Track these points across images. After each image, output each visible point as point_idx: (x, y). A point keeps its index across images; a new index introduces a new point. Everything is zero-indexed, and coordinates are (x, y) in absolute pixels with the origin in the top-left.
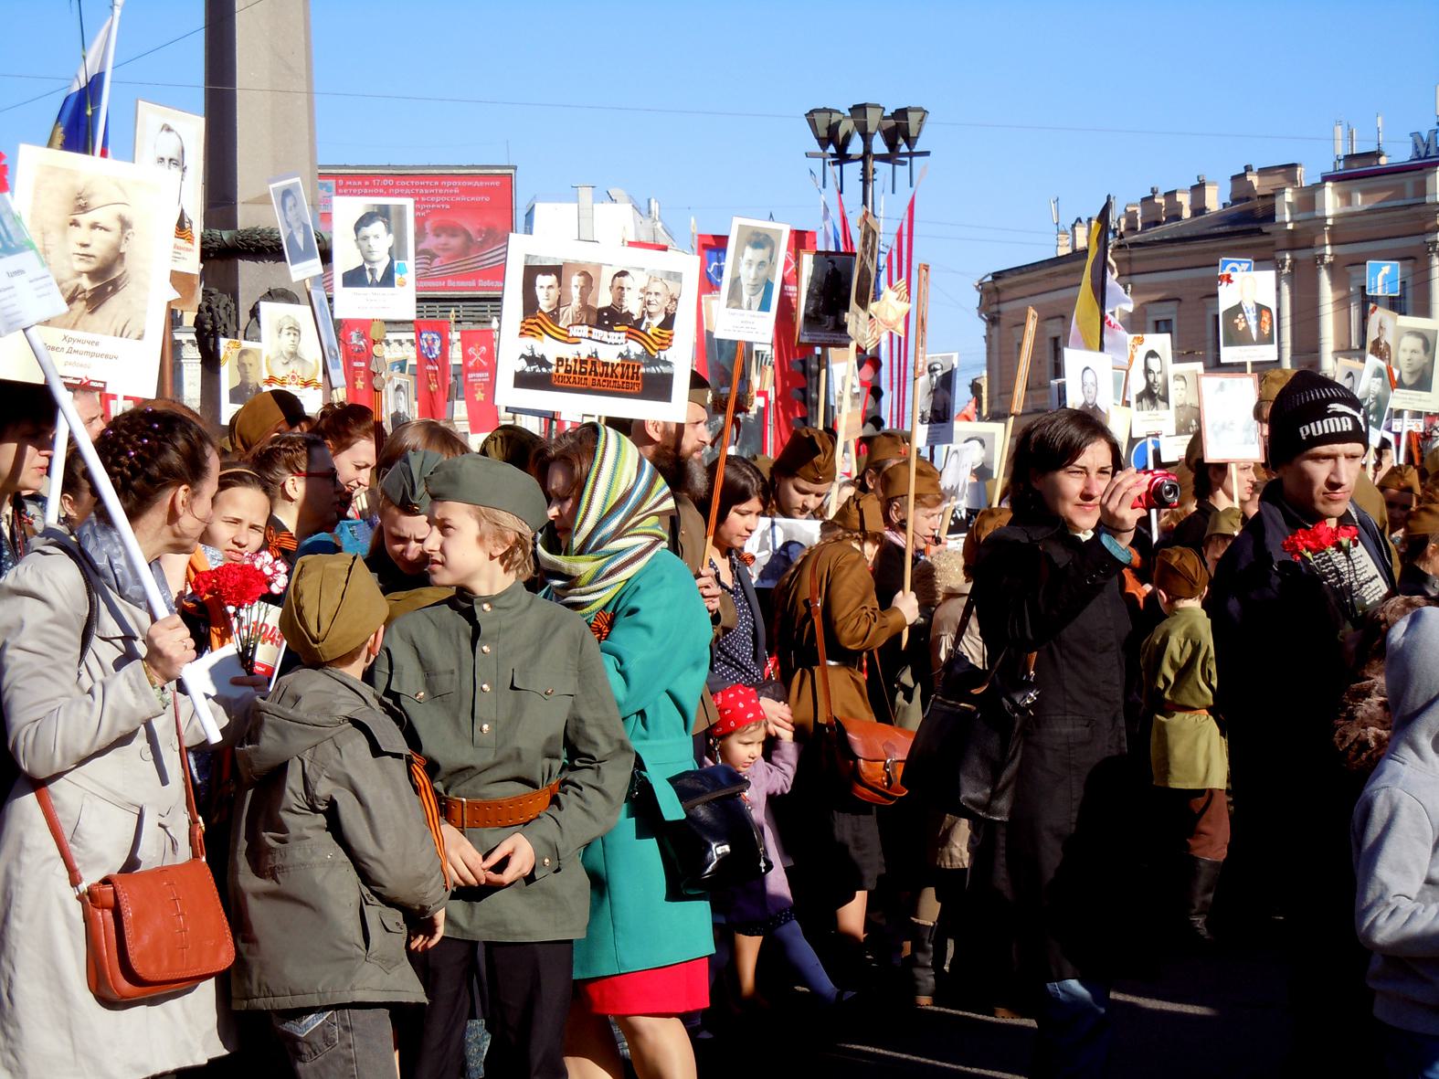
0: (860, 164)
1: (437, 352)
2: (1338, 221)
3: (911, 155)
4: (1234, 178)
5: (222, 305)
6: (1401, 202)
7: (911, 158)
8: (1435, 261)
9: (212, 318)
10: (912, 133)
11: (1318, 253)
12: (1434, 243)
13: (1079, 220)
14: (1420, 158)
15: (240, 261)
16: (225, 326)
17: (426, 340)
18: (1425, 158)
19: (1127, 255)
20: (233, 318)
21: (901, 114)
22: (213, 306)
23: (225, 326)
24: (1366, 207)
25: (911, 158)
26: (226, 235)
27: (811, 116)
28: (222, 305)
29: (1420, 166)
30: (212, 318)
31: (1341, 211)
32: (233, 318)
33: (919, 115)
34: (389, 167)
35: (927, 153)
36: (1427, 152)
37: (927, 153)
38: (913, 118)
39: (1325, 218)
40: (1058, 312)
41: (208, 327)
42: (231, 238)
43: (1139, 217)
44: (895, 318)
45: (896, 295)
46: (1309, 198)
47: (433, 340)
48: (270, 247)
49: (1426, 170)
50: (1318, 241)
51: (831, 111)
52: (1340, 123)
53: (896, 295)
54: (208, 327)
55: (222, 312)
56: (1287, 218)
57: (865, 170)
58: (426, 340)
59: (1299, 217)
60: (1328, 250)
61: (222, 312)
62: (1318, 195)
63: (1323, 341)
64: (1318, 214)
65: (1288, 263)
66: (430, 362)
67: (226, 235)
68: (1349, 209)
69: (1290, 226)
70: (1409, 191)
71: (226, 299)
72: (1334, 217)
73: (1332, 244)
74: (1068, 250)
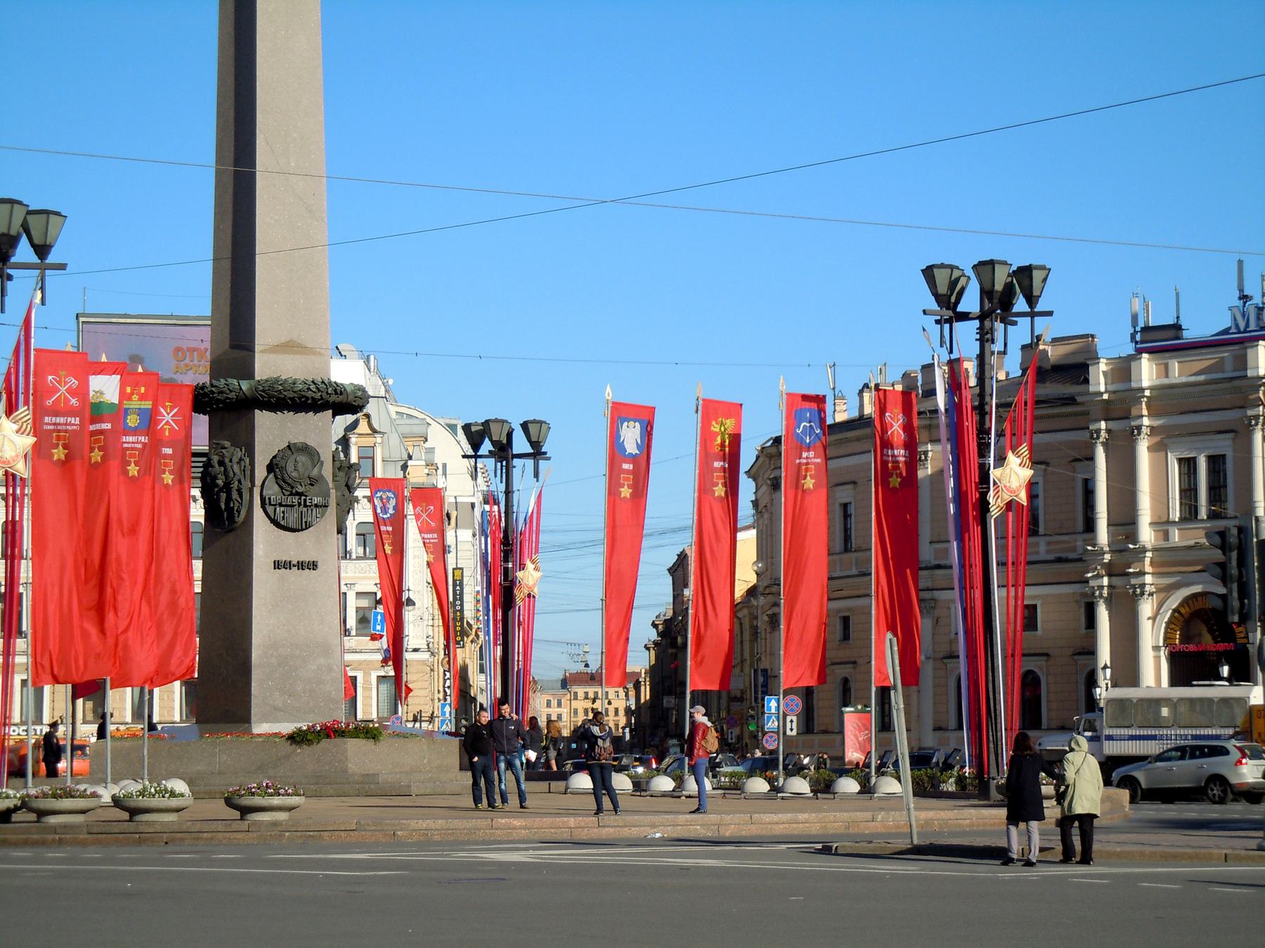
0: (976, 323)
1: (391, 511)
2: (1155, 393)
3: (1032, 315)
4: (1024, 347)
5: (235, 459)
6: (1220, 376)
7: (1032, 318)
8: (1258, 436)
9: (226, 473)
10: (1035, 293)
11: (1133, 423)
12: (1257, 417)
13: (866, 386)
14: (1239, 332)
15: (257, 411)
16: (240, 481)
17: (381, 498)
18: (1245, 332)
19: (928, 422)
20: (248, 473)
21: (1025, 273)
22: (227, 460)
23: (240, 481)
24: (1184, 379)
25: (1032, 318)
26: (245, 385)
27: (929, 273)
28: (235, 459)
29: (1236, 342)
30: (226, 473)
31: (1157, 382)
32: (248, 473)
33: (1044, 273)
34: (171, 317)
35: (1050, 314)
36: (1247, 325)
37: (1050, 314)
38: (1037, 276)
39: (1142, 390)
40: (847, 478)
41: (220, 482)
42: (250, 389)
43: (919, 383)
44: (13, 454)
45: (1018, 461)
46: (1123, 369)
47: (388, 499)
48: (292, 399)
49: (1247, 344)
50: (1134, 412)
51: (952, 267)
52: (1136, 295)
53: (1018, 461)
54: (220, 482)
55: (236, 468)
56: (1102, 389)
57: (981, 328)
58: (381, 498)
59: (1111, 388)
60: (1146, 421)
61: (236, 468)
62: (1134, 364)
63: (1140, 512)
64: (1134, 385)
65: (1103, 434)
66: (385, 522)
67: (245, 385)
68: (1166, 381)
69: (1106, 397)
70: (1229, 365)
71: (239, 453)
72: (1151, 388)
73: (1149, 416)
74: (855, 414)
